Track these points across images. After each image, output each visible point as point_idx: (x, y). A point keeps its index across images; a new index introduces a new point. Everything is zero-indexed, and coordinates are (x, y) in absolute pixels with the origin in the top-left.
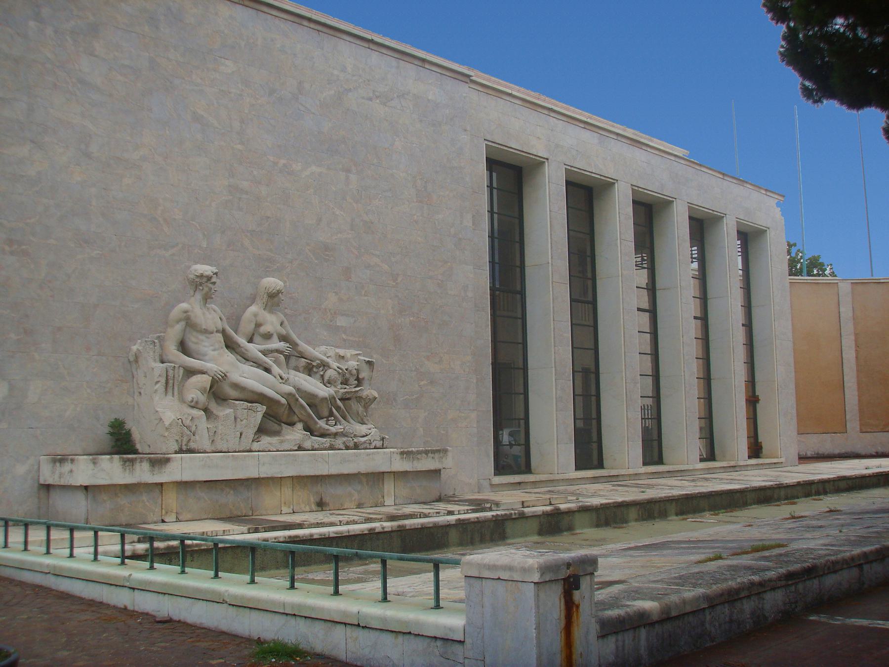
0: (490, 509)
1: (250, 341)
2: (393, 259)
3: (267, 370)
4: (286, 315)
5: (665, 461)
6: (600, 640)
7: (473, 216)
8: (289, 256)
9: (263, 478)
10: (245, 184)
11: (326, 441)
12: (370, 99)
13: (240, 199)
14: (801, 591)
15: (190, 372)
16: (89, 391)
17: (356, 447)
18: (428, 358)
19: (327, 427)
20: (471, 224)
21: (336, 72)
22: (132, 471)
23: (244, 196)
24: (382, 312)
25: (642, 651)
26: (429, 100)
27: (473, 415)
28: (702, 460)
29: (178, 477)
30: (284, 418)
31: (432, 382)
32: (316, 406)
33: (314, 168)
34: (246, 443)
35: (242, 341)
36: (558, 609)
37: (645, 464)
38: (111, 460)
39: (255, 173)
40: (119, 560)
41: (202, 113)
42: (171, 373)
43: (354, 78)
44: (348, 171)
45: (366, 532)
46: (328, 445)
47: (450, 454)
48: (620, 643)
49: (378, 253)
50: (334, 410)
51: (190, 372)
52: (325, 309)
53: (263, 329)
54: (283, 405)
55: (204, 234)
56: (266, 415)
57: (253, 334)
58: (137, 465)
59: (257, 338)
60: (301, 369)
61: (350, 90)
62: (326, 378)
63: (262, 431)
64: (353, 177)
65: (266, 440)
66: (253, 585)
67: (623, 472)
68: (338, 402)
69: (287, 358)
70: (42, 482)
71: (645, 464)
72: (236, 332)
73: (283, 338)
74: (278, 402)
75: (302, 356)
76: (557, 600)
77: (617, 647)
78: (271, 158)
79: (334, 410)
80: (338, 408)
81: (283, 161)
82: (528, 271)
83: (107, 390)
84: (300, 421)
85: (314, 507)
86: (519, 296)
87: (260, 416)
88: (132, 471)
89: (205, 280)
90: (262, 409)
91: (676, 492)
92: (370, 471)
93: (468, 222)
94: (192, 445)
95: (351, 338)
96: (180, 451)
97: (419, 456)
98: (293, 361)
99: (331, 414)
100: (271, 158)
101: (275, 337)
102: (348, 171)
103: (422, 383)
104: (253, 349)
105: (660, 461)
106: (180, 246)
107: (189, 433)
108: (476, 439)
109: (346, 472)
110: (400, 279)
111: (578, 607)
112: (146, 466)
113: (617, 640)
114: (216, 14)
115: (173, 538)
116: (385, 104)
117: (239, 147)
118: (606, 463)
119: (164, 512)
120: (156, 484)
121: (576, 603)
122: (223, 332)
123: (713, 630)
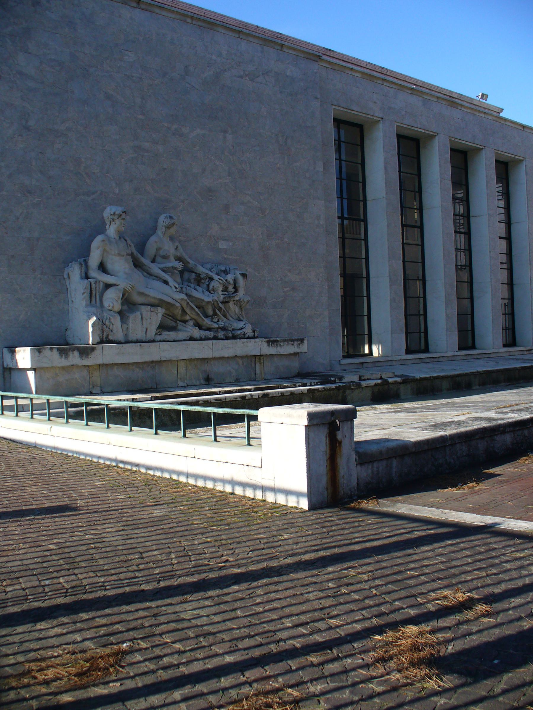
0: (335, 382)
1: (153, 261)
2: (262, 198)
3: (166, 282)
4: (180, 241)
5: (517, 345)
6: (359, 467)
7: (324, 164)
8: (182, 197)
9: (164, 361)
10: (147, 145)
11: (211, 334)
12: (241, 77)
13: (143, 156)
14: (526, 435)
15: (108, 286)
16: (36, 301)
17: (234, 337)
18: (290, 271)
19: (211, 323)
20: (321, 169)
21: (214, 57)
22: (67, 357)
23: (146, 154)
24: (254, 237)
25: (394, 475)
26: (287, 76)
27: (326, 313)
28: (505, 346)
29: (100, 362)
30: (179, 317)
31: (293, 289)
32: (203, 308)
33: (199, 131)
34: (151, 334)
35: (146, 261)
36: (324, 445)
37: (460, 348)
38: (51, 349)
39: (154, 136)
40: (46, 418)
41: (112, 93)
42: (93, 286)
43: (228, 61)
44: (225, 132)
45: (12, 380)
46: (212, 336)
47: (306, 342)
48: (375, 469)
49: (249, 193)
50: (217, 311)
51: (108, 286)
52: (210, 236)
53: (161, 253)
54: (177, 307)
55: (116, 183)
56: (164, 316)
57: (155, 256)
58: (71, 354)
59: (158, 259)
60: (192, 281)
61: (225, 71)
62: (211, 287)
63: (162, 327)
64: (230, 137)
65: (166, 334)
66: (132, 432)
67: (442, 355)
68: (220, 305)
69: (182, 273)
70: (5, 366)
71: (460, 348)
72: (142, 254)
73: (179, 259)
74: (173, 305)
75: (191, 271)
76: (324, 439)
77: (373, 472)
78: (166, 125)
79: (217, 311)
80: (220, 309)
81: (175, 127)
82: (369, 204)
83: (48, 300)
84: (192, 319)
85: (203, 382)
86: (362, 223)
87: (160, 316)
88: (67, 357)
89: (116, 217)
90: (161, 311)
91: (480, 369)
92: (244, 354)
93: (320, 168)
94: (111, 338)
95: (230, 257)
96: (102, 342)
97: (282, 344)
98: (186, 275)
99: (215, 314)
100: (166, 125)
101: (172, 259)
102: (225, 132)
103: (285, 290)
104: (155, 269)
105: (473, 347)
106: (99, 192)
107: (108, 329)
108: (328, 330)
109: (226, 356)
110: (267, 212)
111: (340, 443)
112: (76, 353)
113: (373, 467)
114: (120, 16)
115: (103, 405)
116: (252, 80)
117: (141, 117)
118: (431, 348)
119: (91, 386)
120: (85, 366)
121: (339, 440)
122: (132, 255)
123: (452, 461)
